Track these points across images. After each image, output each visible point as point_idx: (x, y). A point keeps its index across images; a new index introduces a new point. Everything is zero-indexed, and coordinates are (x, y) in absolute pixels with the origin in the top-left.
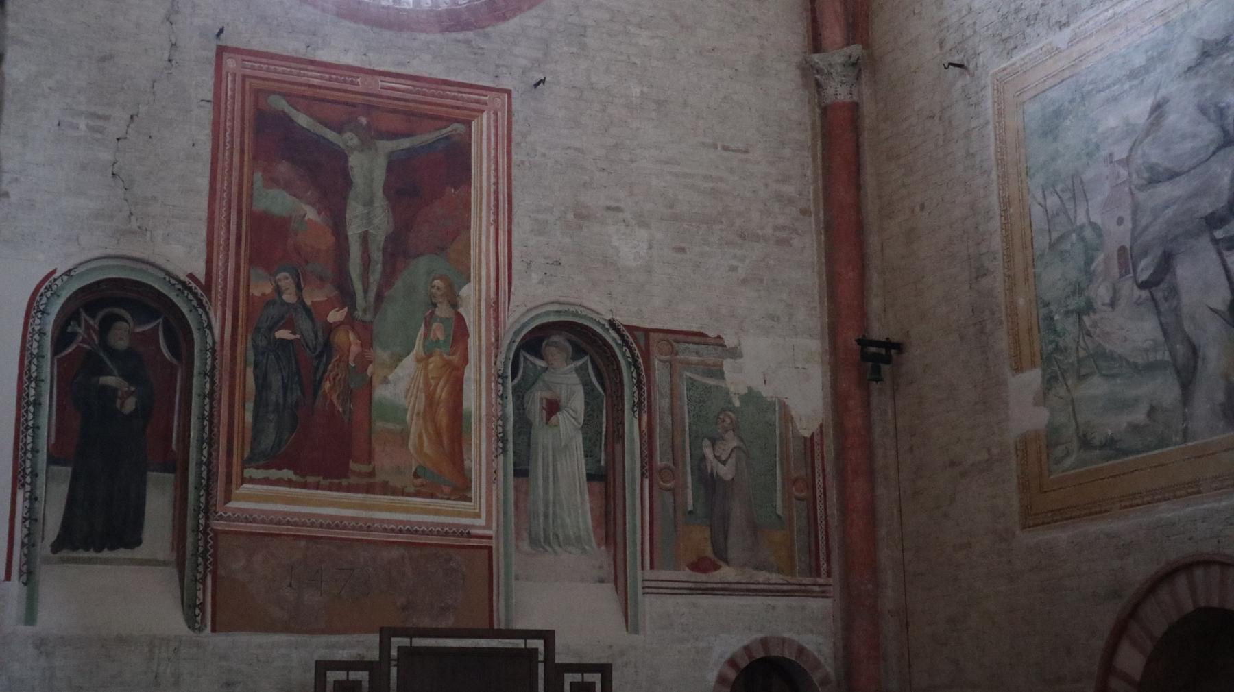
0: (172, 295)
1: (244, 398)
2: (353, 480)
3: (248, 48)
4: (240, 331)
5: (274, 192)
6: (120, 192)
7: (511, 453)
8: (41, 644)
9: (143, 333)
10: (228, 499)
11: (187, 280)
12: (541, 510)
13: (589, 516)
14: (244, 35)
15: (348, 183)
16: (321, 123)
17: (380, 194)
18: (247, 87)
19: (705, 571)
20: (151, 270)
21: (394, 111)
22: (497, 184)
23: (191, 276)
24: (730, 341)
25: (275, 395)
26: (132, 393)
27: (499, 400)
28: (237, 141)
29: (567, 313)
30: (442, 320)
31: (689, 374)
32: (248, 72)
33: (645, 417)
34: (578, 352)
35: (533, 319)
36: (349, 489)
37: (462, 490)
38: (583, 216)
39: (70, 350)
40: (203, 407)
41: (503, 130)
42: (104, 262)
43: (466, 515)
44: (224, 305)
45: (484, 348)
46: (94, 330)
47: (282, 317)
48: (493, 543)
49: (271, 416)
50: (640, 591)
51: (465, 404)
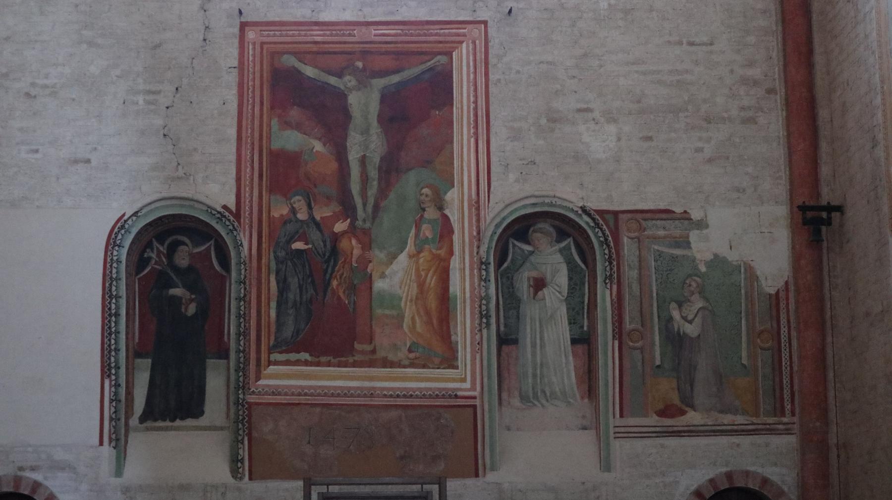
0: (213, 223)
1: (269, 298)
2: (358, 357)
3: (265, 20)
6: (170, 147)
7: (494, 327)
8: (126, 490)
9: (200, 253)
10: (258, 378)
11: (222, 210)
12: (530, 371)
13: (573, 374)
15: (347, 116)
17: (375, 123)
18: (265, 52)
19: (672, 416)
20: (196, 205)
21: (387, 53)
22: (476, 102)
23: (225, 207)
24: (696, 215)
26: (192, 300)
27: (483, 283)
28: (258, 93)
29: (543, 204)
31: (656, 247)
33: (615, 287)
34: (562, 235)
35: (511, 213)
36: (355, 365)
37: (450, 361)
38: (554, 118)
39: (146, 272)
40: (239, 308)
41: (480, 56)
42: (169, 202)
43: (454, 380)
44: (251, 227)
45: (467, 240)
46: (163, 254)
48: (478, 402)
49: (291, 311)
50: (612, 435)
51: (451, 289)
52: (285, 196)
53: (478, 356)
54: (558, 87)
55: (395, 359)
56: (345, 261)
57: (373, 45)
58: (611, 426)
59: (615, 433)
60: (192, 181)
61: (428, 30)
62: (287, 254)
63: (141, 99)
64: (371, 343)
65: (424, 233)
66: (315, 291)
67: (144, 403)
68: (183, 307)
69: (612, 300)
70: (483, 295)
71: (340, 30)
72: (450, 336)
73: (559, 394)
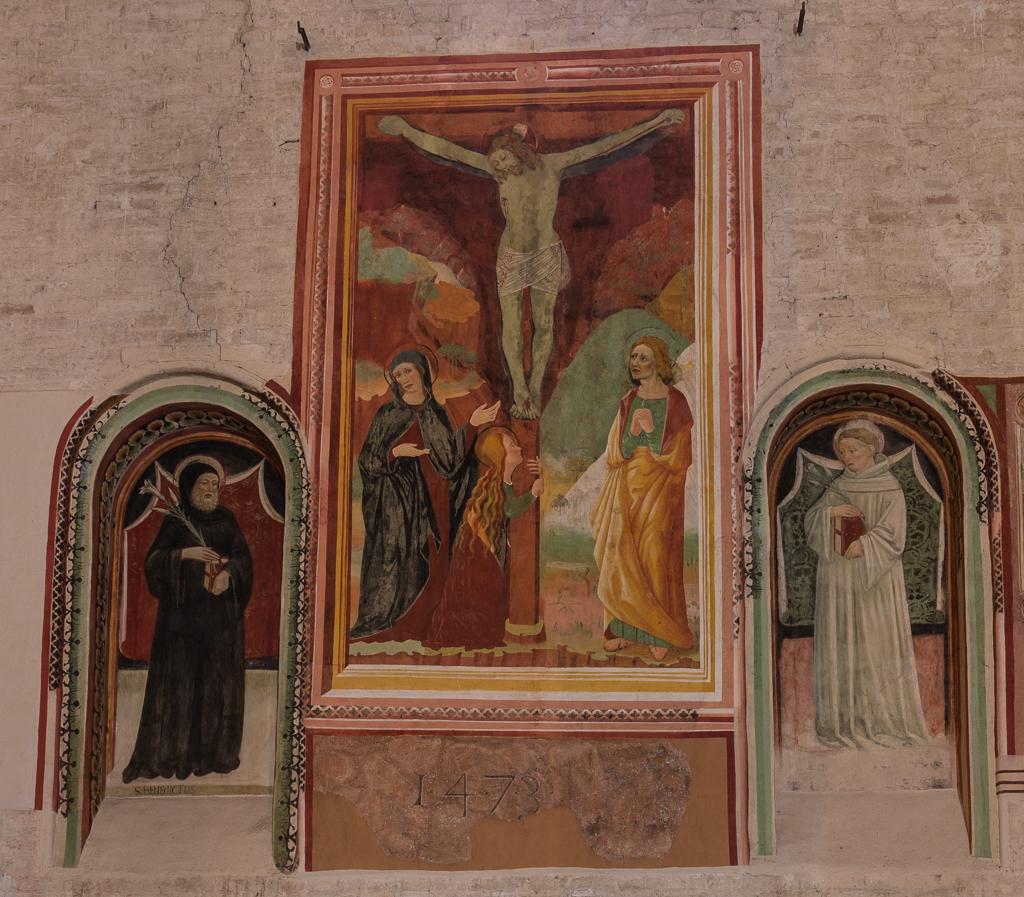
0: (254, 418)
2: (512, 648)
4: (342, 451)
5: (389, 252)
6: (175, 281)
9: (238, 485)
10: (326, 686)
13: (916, 688)
14: (341, 40)
15: (499, 221)
16: (457, 143)
17: (548, 231)
21: (571, 108)
22: (736, 189)
23: (272, 384)
25: (394, 536)
27: (747, 515)
29: (860, 371)
30: (649, 404)
32: (351, 90)
33: (998, 517)
36: (505, 661)
37: (684, 651)
38: (884, 217)
39: (142, 519)
41: (746, 108)
43: (690, 688)
46: (172, 486)
47: (403, 426)
52: (381, 361)
53: (736, 644)
54: (891, 160)
55: (582, 651)
56: (491, 475)
57: (548, 95)
58: (992, 771)
59: (998, 784)
60: (213, 342)
61: (649, 65)
62: (384, 465)
63: (125, 199)
64: (536, 622)
65: (637, 424)
66: (435, 530)
67: (133, 742)
68: (207, 580)
69: (992, 541)
70: (747, 536)
71: (487, 71)
72: (683, 607)
73: (890, 724)
